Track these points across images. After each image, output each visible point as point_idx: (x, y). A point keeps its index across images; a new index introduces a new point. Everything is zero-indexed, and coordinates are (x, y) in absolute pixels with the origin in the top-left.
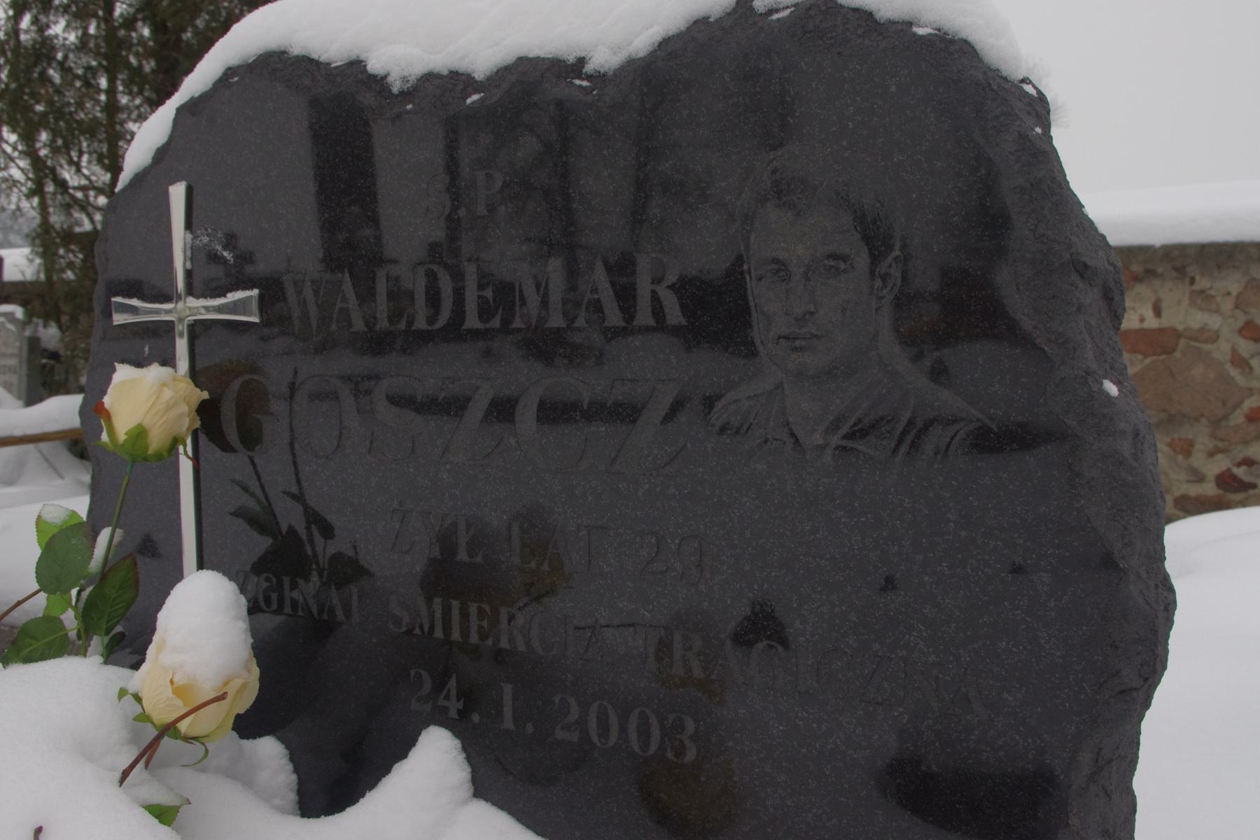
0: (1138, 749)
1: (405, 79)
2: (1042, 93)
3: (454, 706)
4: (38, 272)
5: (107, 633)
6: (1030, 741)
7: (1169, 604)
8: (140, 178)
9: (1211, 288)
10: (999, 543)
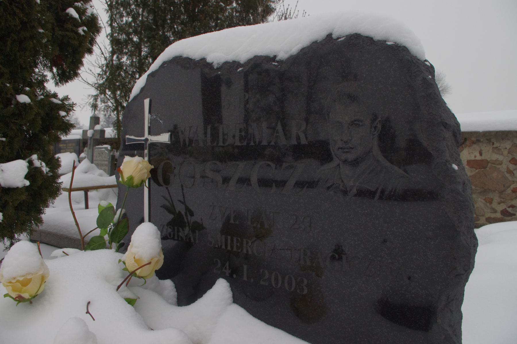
0: (463, 297)
1: (218, 64)
2: (432, 65)
3: (228, 272)
4: (115, 135)
5: (118, 243)
6: (424, 291)
7: (475, 244)
8: (136, 98)
9: (500, 146)
10: (414, 221)
